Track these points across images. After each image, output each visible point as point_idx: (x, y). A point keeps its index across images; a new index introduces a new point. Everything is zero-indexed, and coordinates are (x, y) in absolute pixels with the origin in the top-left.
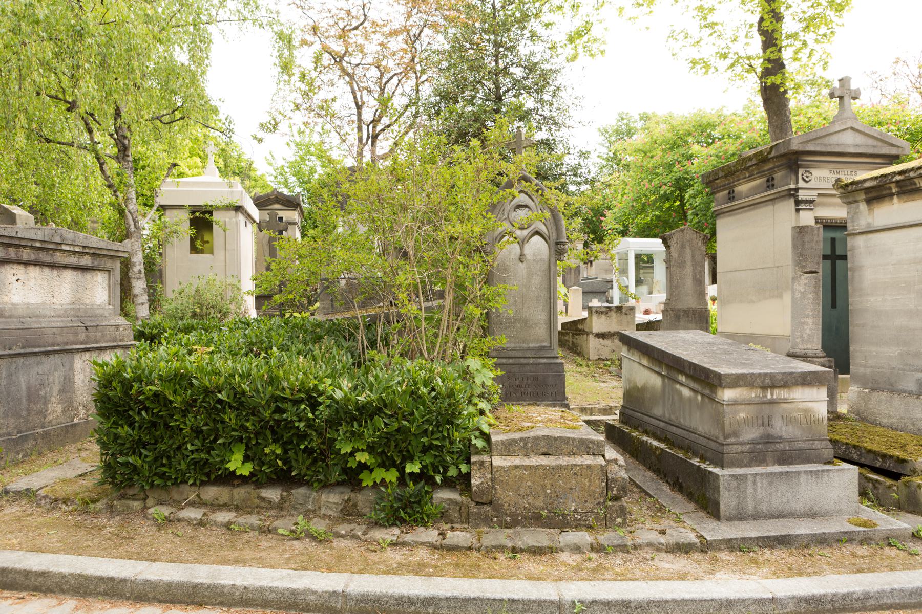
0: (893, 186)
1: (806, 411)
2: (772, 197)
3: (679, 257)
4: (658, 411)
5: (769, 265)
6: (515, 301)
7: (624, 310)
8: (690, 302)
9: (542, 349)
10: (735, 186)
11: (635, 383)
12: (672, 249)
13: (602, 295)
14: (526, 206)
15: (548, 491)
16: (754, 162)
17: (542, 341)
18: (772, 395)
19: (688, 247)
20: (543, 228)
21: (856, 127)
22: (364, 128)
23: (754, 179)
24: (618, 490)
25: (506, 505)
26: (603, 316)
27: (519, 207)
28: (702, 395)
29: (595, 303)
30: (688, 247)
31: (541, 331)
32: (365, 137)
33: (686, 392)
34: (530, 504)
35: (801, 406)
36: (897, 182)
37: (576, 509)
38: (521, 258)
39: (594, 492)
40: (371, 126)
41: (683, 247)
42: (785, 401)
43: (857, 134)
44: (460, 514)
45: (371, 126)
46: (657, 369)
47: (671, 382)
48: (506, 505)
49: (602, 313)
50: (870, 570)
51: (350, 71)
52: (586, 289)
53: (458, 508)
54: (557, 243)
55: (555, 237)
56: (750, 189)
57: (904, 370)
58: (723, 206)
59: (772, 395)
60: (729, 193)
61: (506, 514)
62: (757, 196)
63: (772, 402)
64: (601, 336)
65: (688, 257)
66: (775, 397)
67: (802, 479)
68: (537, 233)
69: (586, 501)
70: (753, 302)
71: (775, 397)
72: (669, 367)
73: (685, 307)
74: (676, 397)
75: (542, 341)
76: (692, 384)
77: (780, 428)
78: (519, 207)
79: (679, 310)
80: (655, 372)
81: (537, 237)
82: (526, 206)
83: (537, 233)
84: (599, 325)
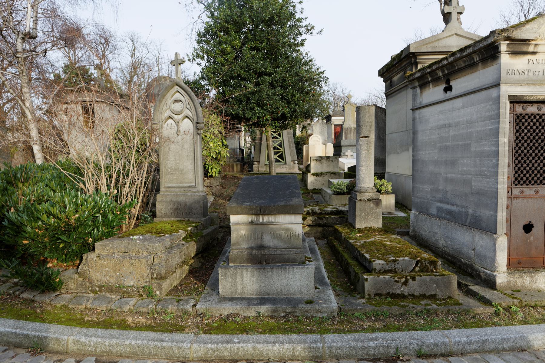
0: (428, 76)
1: (287, 230)
2: (403, 86)
5: (404, 130)
6: (175, 158)
7: (331, 159)
9: (190, 187)
14: (180, 101)
16: (396, 61)
17: (191, 182)
18: (263, 219)
20: (190, 114)
21: (459, 33)
24: (157, 275)
25: (95, 281)
27: (176, 101)
31: (190, 176)
34: (108, 281)
35: (283, 226)
36: (429, 73)
37: (133, 285)
42: (272, 223)
43: (460, 38)
48: (95, 281)
50: (399, 329)
54: (197, 123)
57: (432, 200)
59: (263, 219)
63: (262, 224)
66: (265, 221)
67: (274, 273)
68: (187, 117)
71: (265, 221)
75: (191, 182)
77: (268, 241)
78: (176, 101)
81: (187, 119)
82: (180, 101)
83: (187, 117)
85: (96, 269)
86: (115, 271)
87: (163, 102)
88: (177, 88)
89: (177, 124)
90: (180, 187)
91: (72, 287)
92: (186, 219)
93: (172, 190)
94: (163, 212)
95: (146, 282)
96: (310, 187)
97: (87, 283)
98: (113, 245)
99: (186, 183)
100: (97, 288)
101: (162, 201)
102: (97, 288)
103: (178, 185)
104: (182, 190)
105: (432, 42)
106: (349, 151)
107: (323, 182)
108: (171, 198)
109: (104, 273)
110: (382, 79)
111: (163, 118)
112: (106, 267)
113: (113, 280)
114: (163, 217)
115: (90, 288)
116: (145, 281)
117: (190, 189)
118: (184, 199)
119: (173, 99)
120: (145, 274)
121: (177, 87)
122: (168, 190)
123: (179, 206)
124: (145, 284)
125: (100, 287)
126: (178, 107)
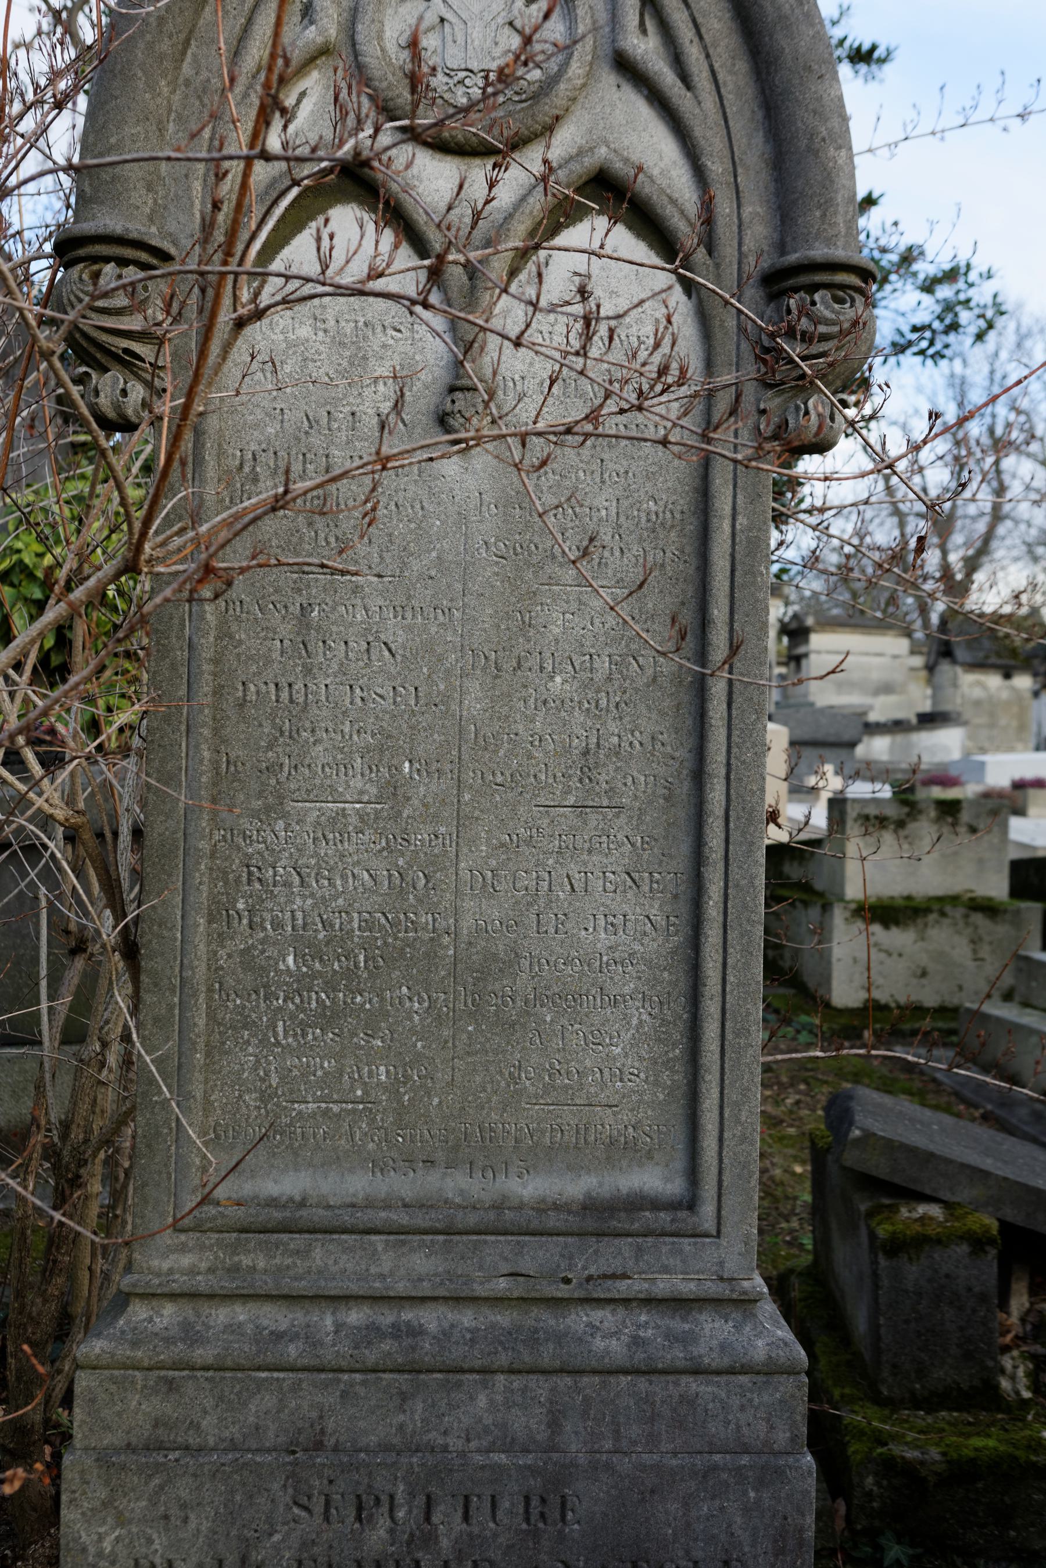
6: (393, 791)
7: (965, 816)
9: (604, 1218)
17: (620, 1150)
20: (651, 151)
26: (888, 837)
31: (610, 1058)
38: (457, 408)
49: (882, 821)
52: (805, 734)
54: (778, 283)
55: (759, 233)
64: (884, 913)
68: (609, 190)
75: (620, 1150)
83: (609, 190)
84: (870, 869)
90: (447, 1227)
93: (331, 1261)
96: (845, 992)
99: (538, 1155)
101: (156, 1449)
103: (404, 1185)
104: (492, 1266)
105: (236, 535)
107: (924, 960)
117: (614, 1254)
118: (527, 1422)
122: (255, 1259)
123: (449, 1525)
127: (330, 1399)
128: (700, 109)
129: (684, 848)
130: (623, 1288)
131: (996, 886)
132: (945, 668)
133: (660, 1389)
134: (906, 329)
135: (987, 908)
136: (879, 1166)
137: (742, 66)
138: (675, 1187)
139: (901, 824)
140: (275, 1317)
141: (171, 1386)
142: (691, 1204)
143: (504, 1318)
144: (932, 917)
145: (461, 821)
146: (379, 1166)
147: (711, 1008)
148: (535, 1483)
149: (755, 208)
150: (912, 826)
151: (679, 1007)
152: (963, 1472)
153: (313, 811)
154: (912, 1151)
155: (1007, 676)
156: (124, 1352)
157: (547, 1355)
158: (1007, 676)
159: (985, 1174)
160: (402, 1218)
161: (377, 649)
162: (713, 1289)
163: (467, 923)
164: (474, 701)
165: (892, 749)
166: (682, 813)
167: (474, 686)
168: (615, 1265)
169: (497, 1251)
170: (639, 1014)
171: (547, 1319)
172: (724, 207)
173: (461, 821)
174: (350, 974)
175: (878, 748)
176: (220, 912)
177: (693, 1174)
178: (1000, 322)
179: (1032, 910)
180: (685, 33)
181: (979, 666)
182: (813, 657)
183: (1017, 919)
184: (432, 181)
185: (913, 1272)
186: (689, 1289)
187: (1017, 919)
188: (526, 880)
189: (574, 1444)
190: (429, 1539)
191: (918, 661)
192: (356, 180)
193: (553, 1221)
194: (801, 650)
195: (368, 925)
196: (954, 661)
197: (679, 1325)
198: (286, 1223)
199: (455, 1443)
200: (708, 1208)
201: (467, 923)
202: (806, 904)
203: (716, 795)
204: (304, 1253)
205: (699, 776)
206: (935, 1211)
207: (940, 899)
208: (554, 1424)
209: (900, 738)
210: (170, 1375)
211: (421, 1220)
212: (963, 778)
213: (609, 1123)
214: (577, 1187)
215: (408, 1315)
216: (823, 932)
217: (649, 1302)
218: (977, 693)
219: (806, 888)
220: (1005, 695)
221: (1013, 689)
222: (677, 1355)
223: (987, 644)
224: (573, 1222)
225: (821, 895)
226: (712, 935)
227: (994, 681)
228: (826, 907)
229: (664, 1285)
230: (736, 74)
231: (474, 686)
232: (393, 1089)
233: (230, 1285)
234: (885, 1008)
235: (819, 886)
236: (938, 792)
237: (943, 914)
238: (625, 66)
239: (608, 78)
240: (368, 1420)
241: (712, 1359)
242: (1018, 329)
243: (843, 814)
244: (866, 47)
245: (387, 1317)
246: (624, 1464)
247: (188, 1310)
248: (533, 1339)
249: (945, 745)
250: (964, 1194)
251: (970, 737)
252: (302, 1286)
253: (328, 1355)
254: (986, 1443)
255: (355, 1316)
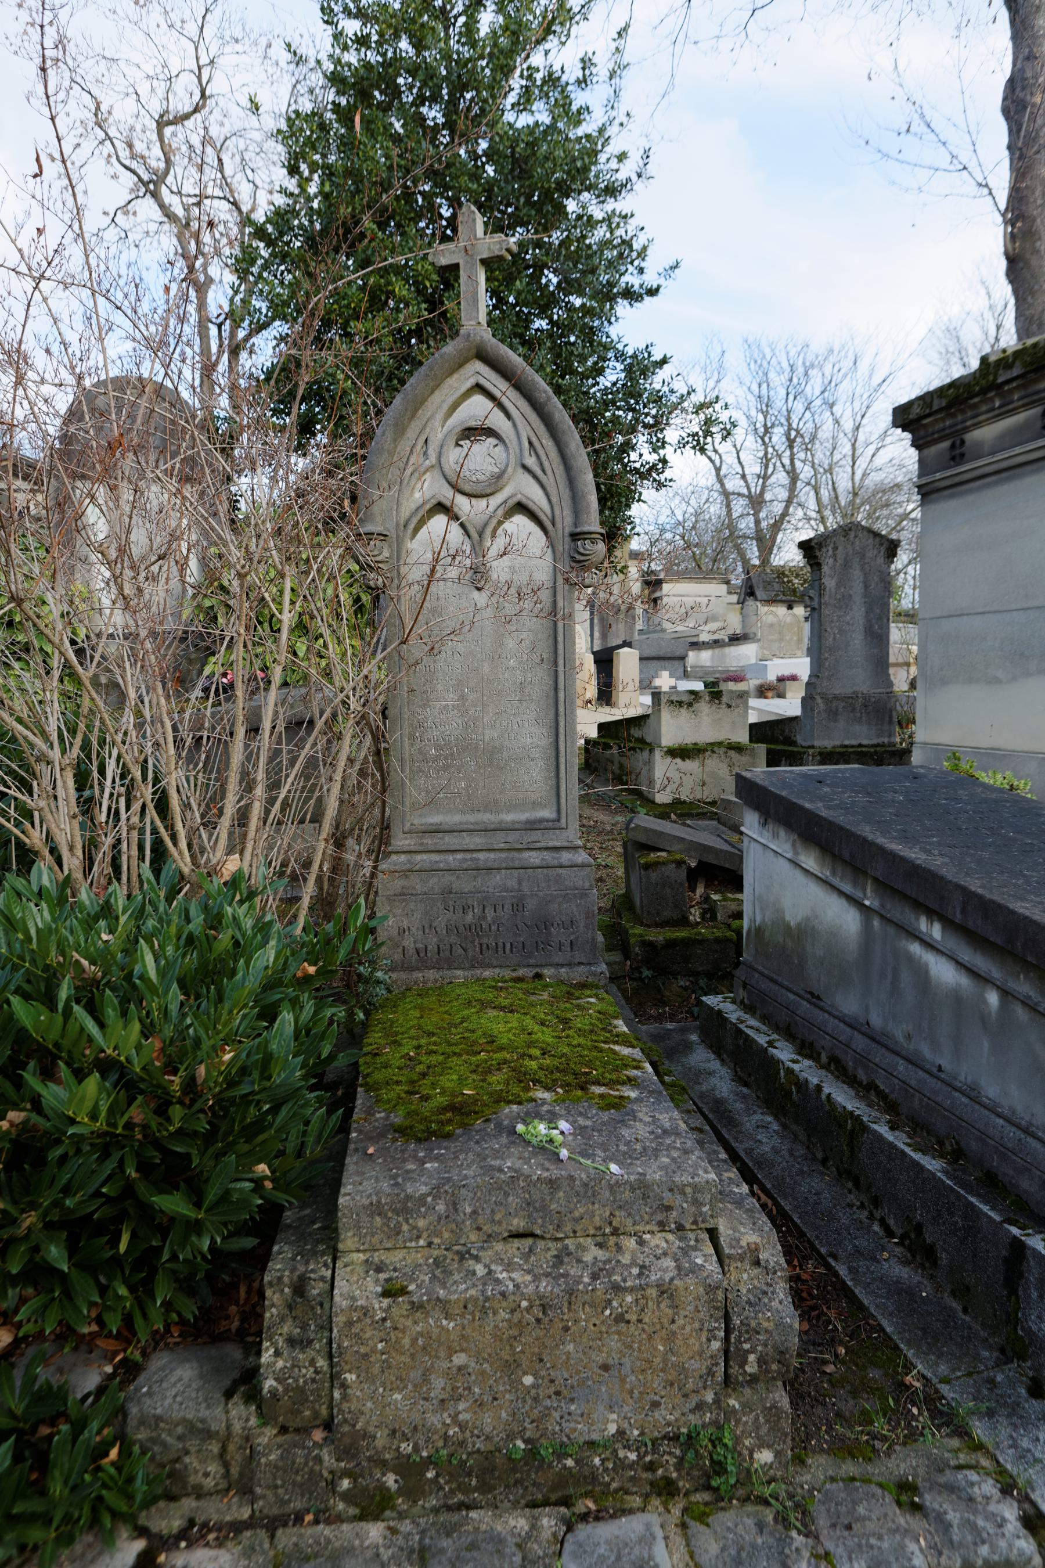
3: (838, 585)
4: (848, 1004)
6: (462, 698)
8: (856, 680)
9: (532, 826)
10: (967, 430)
11: (779, 911)
12: (826, 569)
13: (676, 663)
14: (490, 432)
15: (528, 1380)
16: (1016, 371)
17: (536, 805)
19: (856, 565)
22: (213, 331)
23: (1013, 412)
24: (761, 1361)
26: (684, 711)
27: (472, 433)
28: (1005, 993)
29: (665, 681)
30: (856, 565)
31: (533, 777)
32: (214, 348)
33: (943, 972)
34: (463, 1426)
37: (621, 1433)
39: (682, 1370)
40: (227, 326)
41: (846, 565)
44: (226, 1465)
45: (227, 326)
46: (847, 888)
47: (891, 930)
49: (680, 703)
51: (180, 212)
53: (215, 1448)
54: (575, 537)
55: (569, 520)
56: (1003, 436)
58: (938, 476)
60: (953, 446)
61: (383, 1464)
62: (1018, 450)
65: (857, 589)
69: (656, 1405)
70: (997, 681)
72: (883, 886)
73: (849, 691)
74: (906, 978)
75: (536, 805)
76: (967, 955)
78: (472, 433)
79: (836, 698)
80: (841, 893)
82: (490, 432)
84: (673, 729)
85: (386, 1366)
86: (511, 1367)
87: (411, 433)
88: (478, 371)
89: (476, 535)
91: (209, 1483)
92: (529, 973)
93: (450, 841)
94: (408, 942)
95: (700, 1407)
97: (328, 1459)
98: (455, 1206)
99: (512, 807)
100: (391, 1480)
102: (391, 1480)
103: (471, 818)
104: (498, 841)
106: (665, 674)
108: (448, 879)
109: (438, 1385)
110: (908, 436)
111: (408, 507)
112: (451, 1352)
113: (492, 1422)
114: (412, 969)
115: (346, 1484)
116: (694, 1400)
118: (512, 883)
119: (451, 422)
120: (698, 1366)
121: (478, 366)
122: (429, 841)
123: (490, 913)
124: (694, 1419)
125: (409, 1469)
126: (482, 458)
127: (453, 878)
128: (549, 481)
129: (553, 712)
130: (538, 845)
131: (743, 737)
132: (750, 602)
133: (550, 872)
134: (685, 435)
135: (738, 748)
136: (642, 838)
137: (562, 467)
138: (553, 815)
139: (690, 705)
140: (435, 857)
141: (407, 877)
142: (559, 820)
143: (503, 855)
144: (707, 754)
145: (484, 706)
146: (463, 812)
147: (562, 760)
148: (515, 900)
149: (568, 513)
150: (696, 705)
151: (553, 760)
152: (671, 944)
153: (438, 705)
154: (655, 831)
155: (790, 607)
156: (392, 868)
157: (517, 864)
158: (790, 607)
159: (683, 839)
160: (472, 827)
161: (456, 655)
162: (566, 844)
163: (487, 738)
164: (486, 669)
165: (712, 658)
166: (551, 701)
167: (486, 664)
168: (536, 839)
169: (500, 835)
170: (541, 763)
171: (516, 855)
172: (558, 512)
173: (484, 706)
174: (452, 754)
175: (703, 658)
176: (412, 737)
177: (559, 811)
178: (735, 431)
179: (762, 749)
180: (544, 458)
181: (772, 601)
182: (665, 600)
183: (753, 753)
184: (462, 503)
185: (654, 876)
186: (558, 844)
187: (753, 753)
188: (504, 723)
189: (526, 889)
190: (484, 918)
191: (734, 598)
192: (441, 508)
193: (517, 826)
194: (657, 594)
195: (457, 739)
196: (756, 599)
197: (556, 855)
198: (437, 830)
199: (491, 890)
200: (563, 821)
201: (487, 738)
202: (641, 750)
203: (561, 695)
204: (442, 838)
205: (556, 689)
206: (664, 854)
207: (712, 744)
208: (520, 883)
209: (717, 651)
210: (406, 873)
211: (477, 827)
212: (748, 676)
213: (533, 797)
214: (523, 817)
215: (475, 855)
216: (650, 763)
217: (547, 849)
218: (770, 619)
219: (642, 740)
220: (789, 620)
221: (794, 615)
222: (555, 862)
223: (776, 586)
224: (523, 826)
225: (649, 744)
226: (562, 738)
227: (781, 610)
228: (651, 751)
229: (551, 844)
230: (560, 470)
231: (486, 664)
232: (466, 789)
233: (421, 848)
234: (685, 802)
235: (648, 740)
236: (732, 686)
237: (713, 752)
238: (524, 467)
239: (521, 471)
240: (464, 884)
241: (566, 863)
242: (804, 363)
243: (659, 700)
244: (655, 286)
245: (468, 856)
246: (541, 894)
247: (408, 856)
248: (512, 860)
249: (746, 654)
250: (676, 847)
251: (762, 648)
252: (443, 848)
253: (452, 867)
254: (682, 934)
255: (459, 856)
